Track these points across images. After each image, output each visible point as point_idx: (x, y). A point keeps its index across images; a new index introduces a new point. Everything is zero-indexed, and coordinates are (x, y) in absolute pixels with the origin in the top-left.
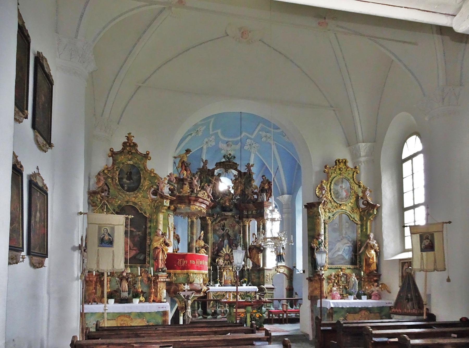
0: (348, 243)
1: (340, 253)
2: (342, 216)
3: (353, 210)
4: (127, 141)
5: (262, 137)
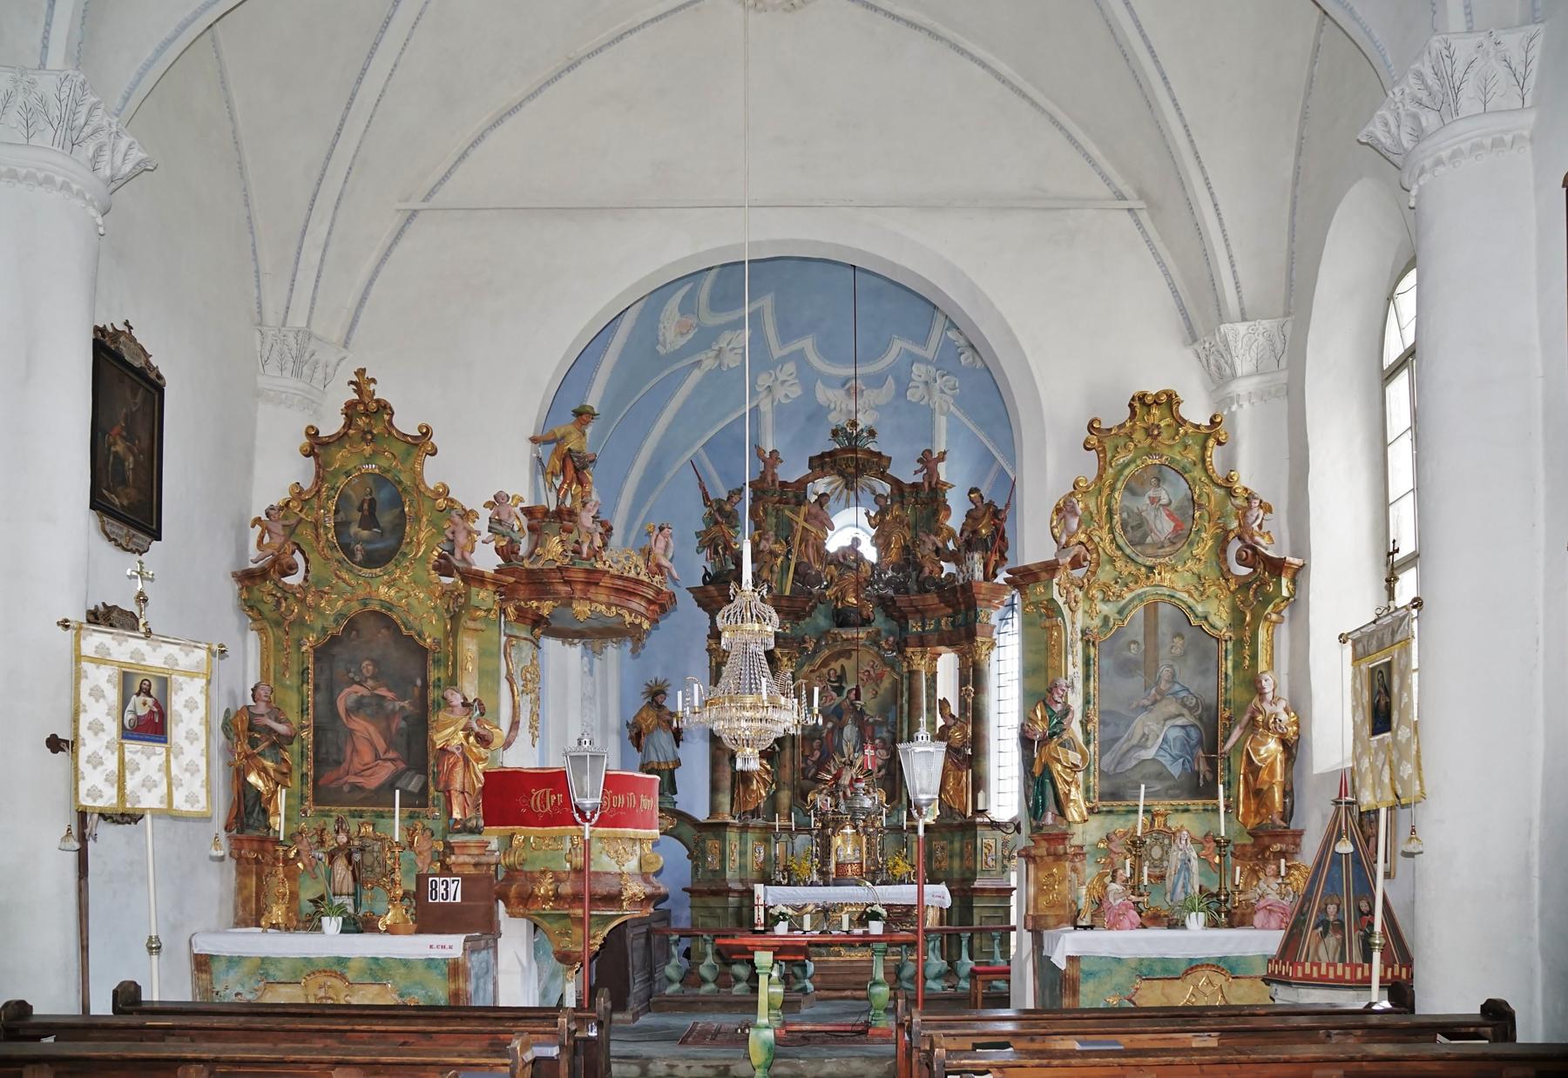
0: (1181, 715)
1: (1149, 754)
2: (1156, 610)
3: (1203, 585)
4: (356, 397)
5: (959, 350)
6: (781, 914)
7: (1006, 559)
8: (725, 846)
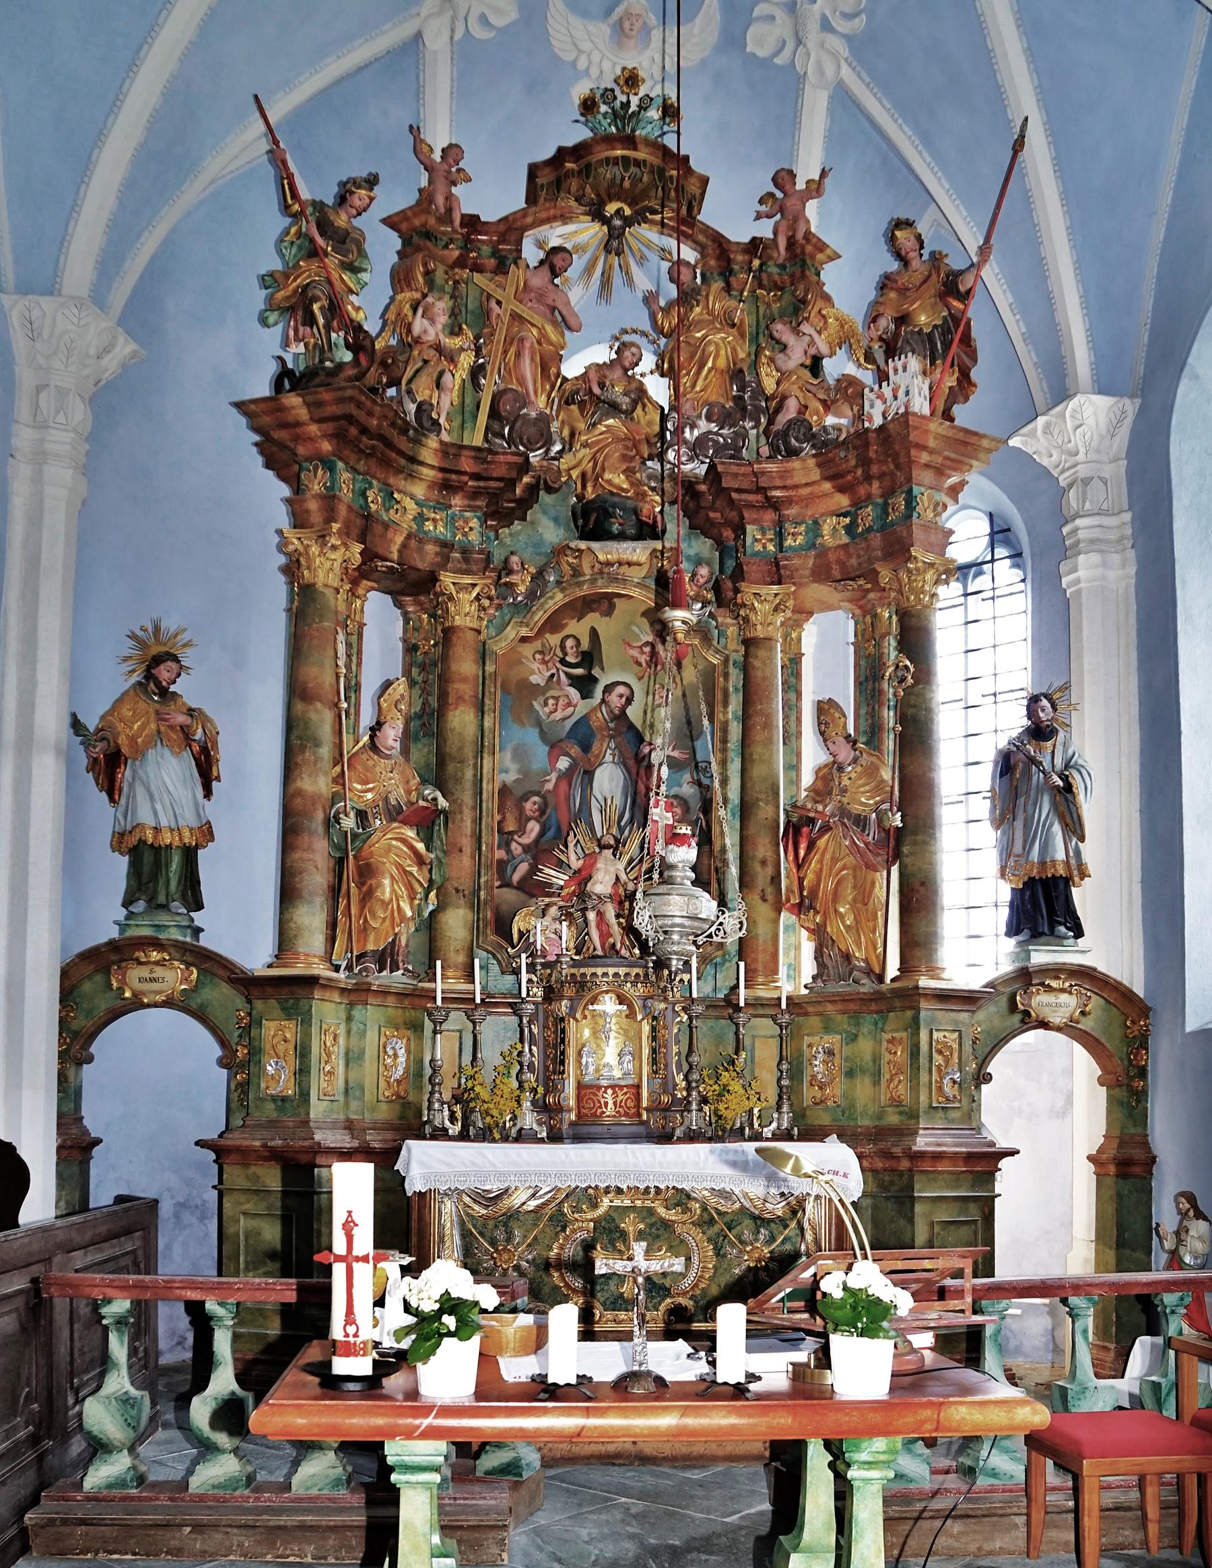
6: (450, 1304)
7: (972, 384)
8: (307, 1035)
